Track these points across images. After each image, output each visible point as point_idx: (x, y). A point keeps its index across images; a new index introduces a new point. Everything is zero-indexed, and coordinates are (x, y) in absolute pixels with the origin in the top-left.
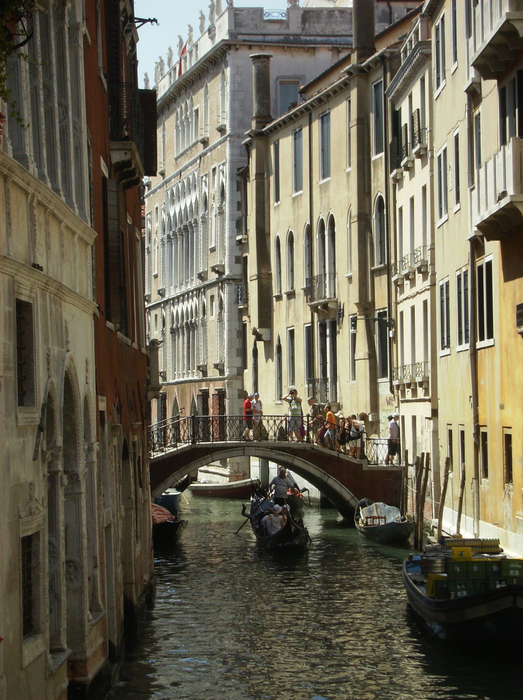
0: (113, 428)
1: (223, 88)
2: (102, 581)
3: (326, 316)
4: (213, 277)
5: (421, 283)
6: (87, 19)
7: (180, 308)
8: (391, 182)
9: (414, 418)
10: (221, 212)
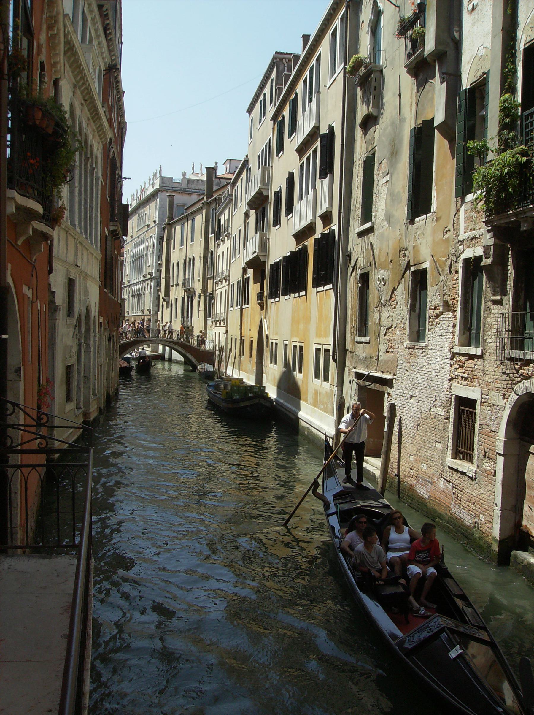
0: (105, 329)
1: (156, 206)
2: (98, 384)
3: (190, 294)
4: (148, 277)
5: (225, 283)
6: (103, 175)
7: (136, 288)
8: (216, 245)
9: (219, 333)
10: (153, 253)
